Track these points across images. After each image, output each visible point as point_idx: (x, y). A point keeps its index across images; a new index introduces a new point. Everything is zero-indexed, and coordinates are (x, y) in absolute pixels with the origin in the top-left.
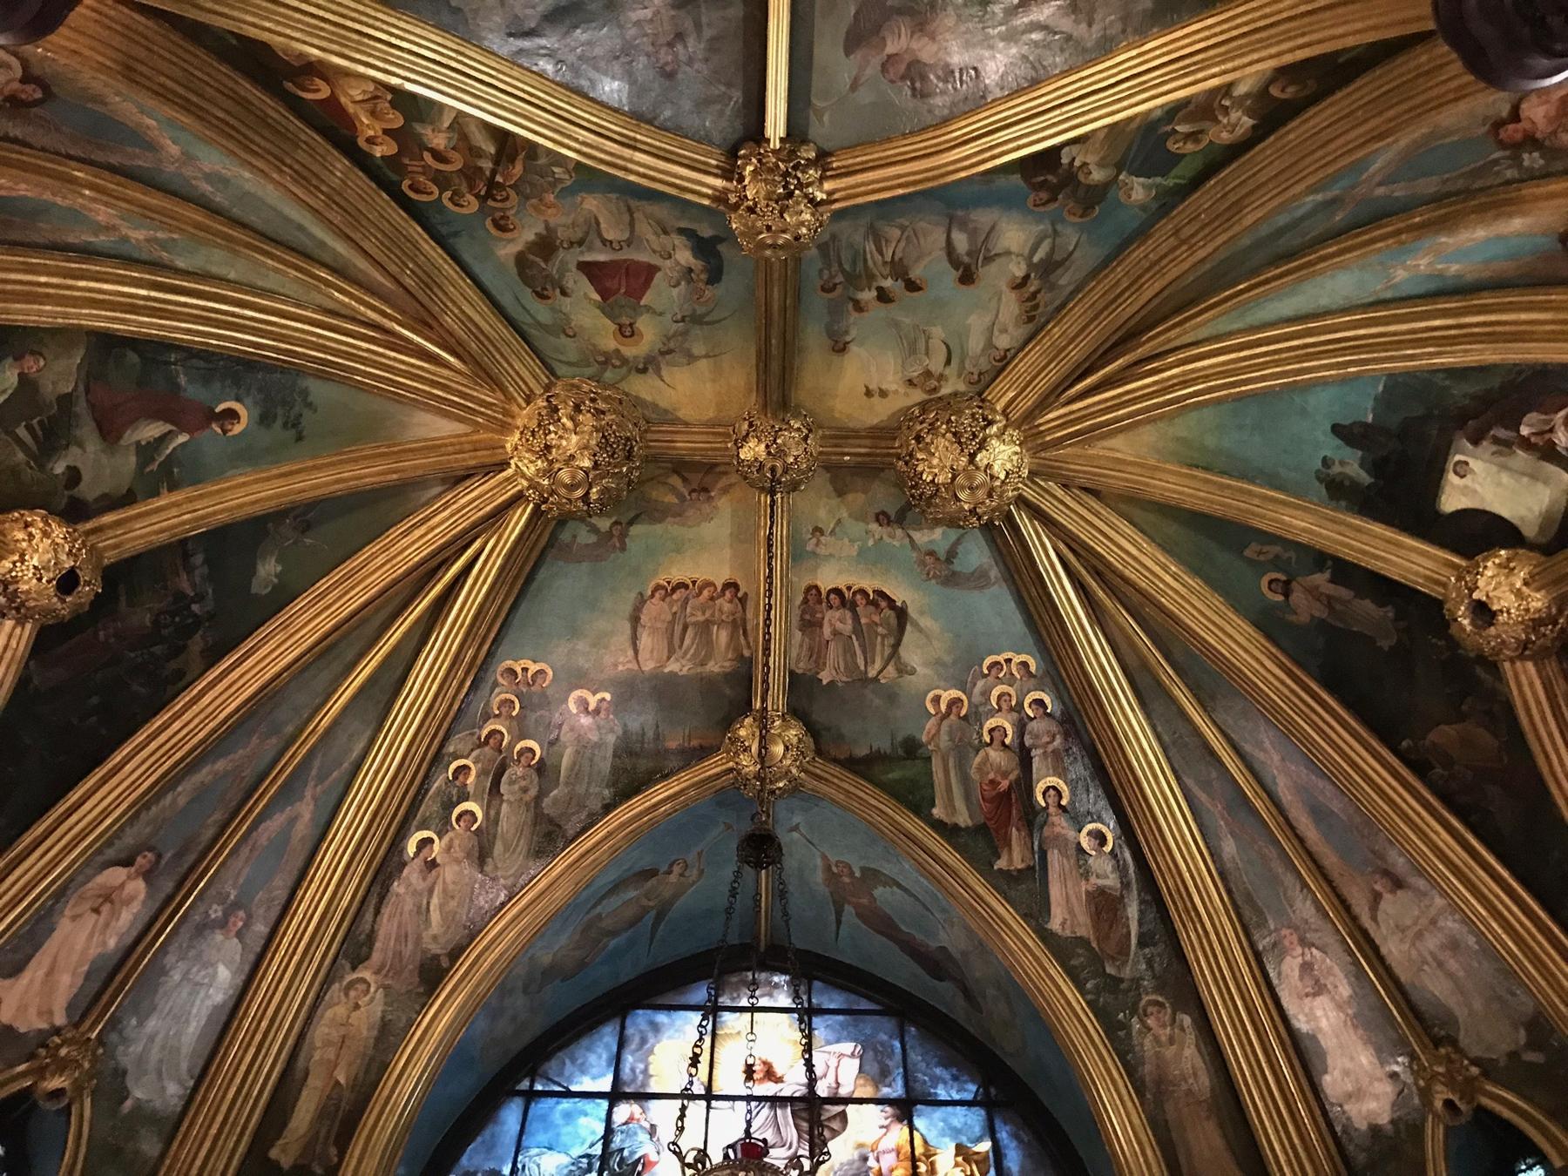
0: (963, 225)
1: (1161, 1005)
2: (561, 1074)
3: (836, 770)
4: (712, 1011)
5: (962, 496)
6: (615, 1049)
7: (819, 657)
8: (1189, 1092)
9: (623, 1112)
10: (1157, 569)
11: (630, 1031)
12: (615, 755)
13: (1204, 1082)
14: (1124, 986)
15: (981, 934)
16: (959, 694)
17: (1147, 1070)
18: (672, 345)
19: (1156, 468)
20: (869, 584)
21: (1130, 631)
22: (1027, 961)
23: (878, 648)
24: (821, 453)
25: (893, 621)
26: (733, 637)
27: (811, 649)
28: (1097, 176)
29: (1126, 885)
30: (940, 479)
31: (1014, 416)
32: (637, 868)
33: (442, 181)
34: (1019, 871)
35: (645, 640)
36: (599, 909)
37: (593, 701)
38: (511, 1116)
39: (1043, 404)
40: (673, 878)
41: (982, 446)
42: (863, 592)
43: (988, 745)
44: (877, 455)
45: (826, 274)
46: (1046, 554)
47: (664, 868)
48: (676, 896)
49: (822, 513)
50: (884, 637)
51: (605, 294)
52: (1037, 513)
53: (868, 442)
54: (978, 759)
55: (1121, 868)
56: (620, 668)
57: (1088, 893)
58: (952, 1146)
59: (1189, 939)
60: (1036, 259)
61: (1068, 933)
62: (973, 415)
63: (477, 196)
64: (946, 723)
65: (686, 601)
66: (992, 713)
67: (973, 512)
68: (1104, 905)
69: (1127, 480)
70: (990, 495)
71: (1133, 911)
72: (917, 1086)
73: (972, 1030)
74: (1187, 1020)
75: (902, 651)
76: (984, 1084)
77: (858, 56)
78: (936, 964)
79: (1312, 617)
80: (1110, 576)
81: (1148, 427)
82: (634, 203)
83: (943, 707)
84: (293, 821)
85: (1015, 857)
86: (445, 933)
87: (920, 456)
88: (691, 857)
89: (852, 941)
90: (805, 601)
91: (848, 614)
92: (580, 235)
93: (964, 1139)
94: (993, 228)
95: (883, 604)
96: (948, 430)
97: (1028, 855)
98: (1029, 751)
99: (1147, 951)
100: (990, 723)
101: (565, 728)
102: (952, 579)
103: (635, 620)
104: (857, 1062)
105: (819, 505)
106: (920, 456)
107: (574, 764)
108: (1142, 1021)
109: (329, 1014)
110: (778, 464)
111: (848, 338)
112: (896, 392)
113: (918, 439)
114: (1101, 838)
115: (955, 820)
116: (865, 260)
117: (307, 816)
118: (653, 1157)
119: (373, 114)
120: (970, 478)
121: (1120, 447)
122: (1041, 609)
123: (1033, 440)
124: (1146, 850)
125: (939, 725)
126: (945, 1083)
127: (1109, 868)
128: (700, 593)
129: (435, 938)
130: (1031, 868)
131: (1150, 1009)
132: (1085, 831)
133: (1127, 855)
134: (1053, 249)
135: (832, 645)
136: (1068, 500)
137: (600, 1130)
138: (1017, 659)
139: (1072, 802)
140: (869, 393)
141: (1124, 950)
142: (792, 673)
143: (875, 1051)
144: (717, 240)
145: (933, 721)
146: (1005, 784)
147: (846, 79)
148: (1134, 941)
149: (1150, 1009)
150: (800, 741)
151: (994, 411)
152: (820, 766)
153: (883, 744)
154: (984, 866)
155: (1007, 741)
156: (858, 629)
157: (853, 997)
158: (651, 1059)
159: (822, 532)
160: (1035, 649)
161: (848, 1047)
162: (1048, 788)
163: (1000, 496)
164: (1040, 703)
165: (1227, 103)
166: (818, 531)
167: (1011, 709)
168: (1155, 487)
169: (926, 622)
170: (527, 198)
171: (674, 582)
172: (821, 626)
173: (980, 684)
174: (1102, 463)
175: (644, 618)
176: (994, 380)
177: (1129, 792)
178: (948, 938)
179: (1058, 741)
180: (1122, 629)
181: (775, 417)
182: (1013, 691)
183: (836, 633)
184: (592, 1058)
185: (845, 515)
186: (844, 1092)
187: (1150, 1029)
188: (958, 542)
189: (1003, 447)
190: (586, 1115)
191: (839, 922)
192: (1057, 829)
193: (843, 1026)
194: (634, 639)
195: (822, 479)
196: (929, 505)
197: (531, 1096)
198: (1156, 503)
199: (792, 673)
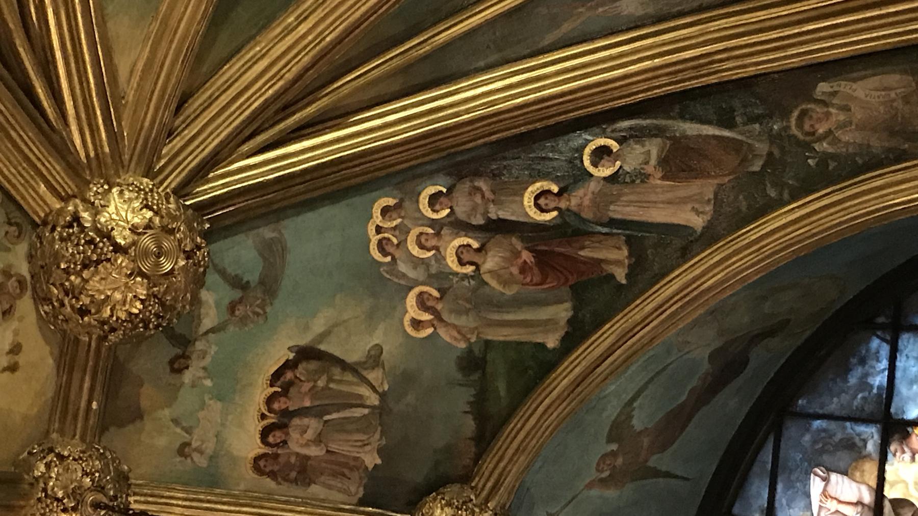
1: (804, 114)
3: (488, 464)
5: (167, 267)
7: (346, 465)
8: (906, 99)
10: (289, 40)
13: (896, 79)
14: (776, 152)
15: (701, 311)
16: (411, 300)
17: (877, 143)
19: (165, 23)
20: (261, 391)
21: (361, 81)
22: (737, 263)
23: (344, 388)
24: (83, 439)
25: (313, 365)
27: (335, 474)
29: (658, 132)
30: (142, 292)
31: (70, 186)
34: (630, 255)
39: (61, 148)
41: (107, 235)
42: (270, 400)
43: (478, 267)
44: (96, 365)
46: (253, 168)
49: (162, 441)
50: (331, 380)
52: (201, 173)
53: (77, 376)
54: (493, 283)
55: (638, 135)
57: (663, 178)
59: (730, 71)
61: (709, 208)
62: (62, 239)
64: (445, 316)
66: (440, 258)
67: (189, 255)
68: (680, 162)
69: (173, 64)
70: (172, 232)
71: (691, 129)
72: (869, 408)
73: (808, 333)
74: (823, 87)
75: (352, 357)
76: (871, 328)
78: (728, 366)
80: (289, 97)
81: (110, 25)
83: (426, 317)
85: (615, 258)
87: (107, 312)
90: (273, 475)
91: (296, 421)
95: (289, 375)
96: (79, 274)
97: (612, 241)
99: (739, 120)
100: (452, 262)
102: (269, 286)
104: (834, 477)
105: (151, 444)
106: (107, 312)
108: (820, 139)
110: (90, 498)
112: (16, 333)
114: (601, 153)
115: (563, 322)
120: (146, 253)
121: (130, 61)
122: (321, 182)
123: (105, 170)
124: (622, 102)
125: (447, 324)
130: (629, 241)
132: (591, 169)
133: (626, 124)
135: (333, 447)
136: (188, 133)
138: (377, 219)
139: (556, 180)
140: (12, 368)
141: (736, 146)
142: (362, 502)
143: (822, 451)
145: (442, 332)
146: (526, 256)
148: (726, 133)
149: (807, 127)
150: (449, 504)
151: (60, 212)
152: (483, 480)
153: (463, 397)
154: (622, 296)
155: (475, 245)
156: (318, 412)
157: (756, 469)
159: (187, 444)
160: (368, 197)
161: (816, 485)
162: (537, 205)
163: (174, 218)
164: (434, 199)
166: (183, 450)
167: (438, 234)
168: (187, 30)
169: (318, 326)
172: (308, 458)
173: (402, 267)
174: (148, 87)
176: (20, 207)
177: (553, 111)
178: (701, 351)
179: (481, 184)
180: (358, 90)
181: (26, 496)
182: (422, 235)
183: (318, 440)
185: (167, 412)
186: (868, 498)
187: (829, 132)
188: (222, 273)
189: (111, 209)
191: (667, 475)
192: (586, 202)
193: (789, 486)
195: (116, 439)
196: (173, 308)
198: (208, 28)
199: (362, 502)
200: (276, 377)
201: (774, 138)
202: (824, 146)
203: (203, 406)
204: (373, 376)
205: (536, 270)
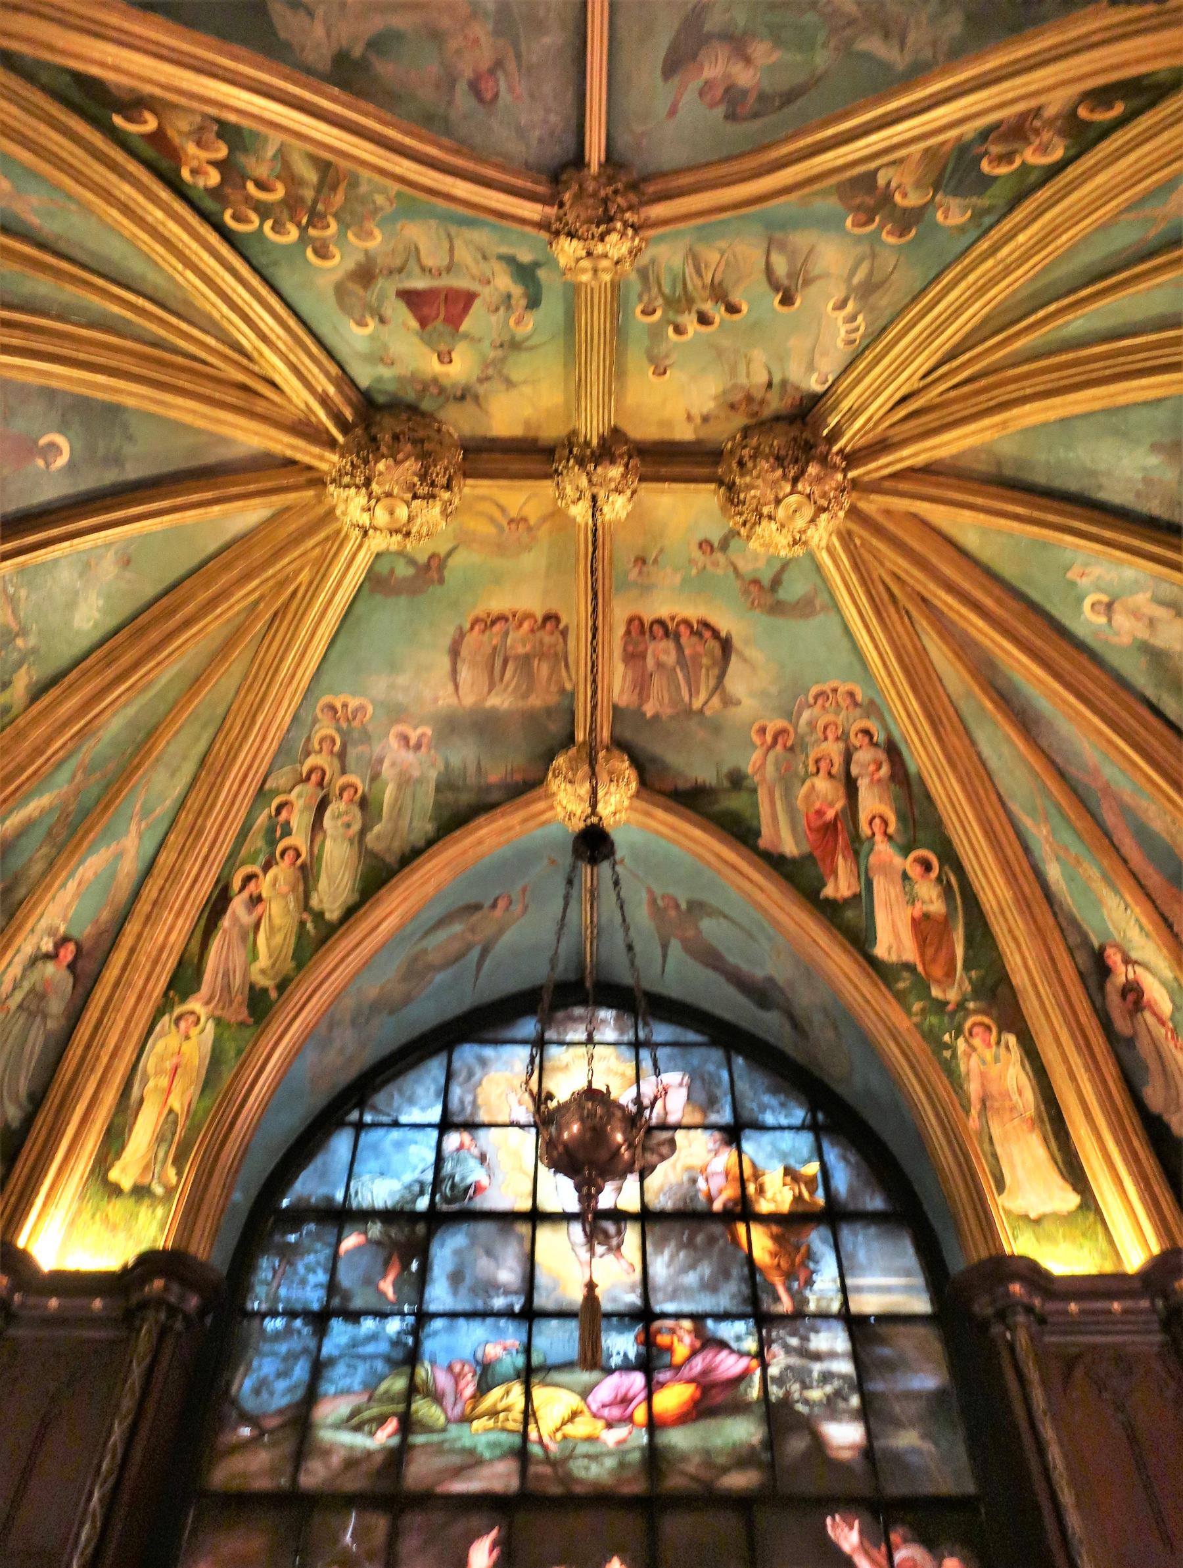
0: (782, 247)
2: (390, 1105)
4: (540, 1044)
6: (442, 1081)
9: (453, 1140)
11: (457, 1064)
12: (438, 790)
18: (490, 371)
26: (553, 671)
28: (913, 200)
32: (461, 903)
33: (264, 211)
35: (465, 674)
36: (425, 943)
37: (414, 737)
38: (341, 1143)
40: (498, 912)
42: (687, 622)
45: (645, 298)
47: (488, 903)
48: (501, 931)
51: (423, 322)
55: (947, 892)
56: (440, 703)
58: (781, 1171)
60: (856, 280)
63: (298, 225)
64: (771, 756)
65: (507, 634)
68: (927, 930)
74: (1012, 1039)
76: (812, 1109)
77: (676, 81)
78: (762, 994)
79: (1135, 639)
82: (453, 230)
83: (769, 738)
84: (119, 856)
86: (273, 965)
88: (516, 893)
89: (678, 975)
90: (628, 632)
92: (398, 262)
93: (792, 1162)
94: (811, 251)
95: (707, 634)
97: (854, 881)
98: (856, 780)
99: (973, 974)
101: (386, 764)
102: (777, 609)
103: (455, 653)
107: (396, 800)
109: (160, 1046)
111: (667, 362)
113: (741, 464)
116: (685, 284)
117: (132, 852)
118: (485, 1182)
119: (199, 144)
126: (773, 1111)
127: (934, 896)
128: (520, 625)
129: (263, 972)
130: (856, 897)
131: (975, 1030)
134: (871, 273)
135: (656, 679)
137: (431, 1157)
143: (703, 1080)
144: (536, 265)
147: (662, 109)
155: (834, 771)
158: (479, 1090)
165: (1037, 123)
167: (837, 739)
169: (752, 653)
170: (348, 227)
171: (495, 614)
175: (464, 652)
183: (660, 665)
184: (420, 1091)
186: (672, 1119)
187: (974, 1049)
190: (416, 1143)
191: (665, 956)
194: (454, 672)
197: (360, 1127)
200: (706, 625)
201: (961, 1005)
202: (961, 1044)
203: (676, 570)
204: (716, 701)
205: (820, 823)
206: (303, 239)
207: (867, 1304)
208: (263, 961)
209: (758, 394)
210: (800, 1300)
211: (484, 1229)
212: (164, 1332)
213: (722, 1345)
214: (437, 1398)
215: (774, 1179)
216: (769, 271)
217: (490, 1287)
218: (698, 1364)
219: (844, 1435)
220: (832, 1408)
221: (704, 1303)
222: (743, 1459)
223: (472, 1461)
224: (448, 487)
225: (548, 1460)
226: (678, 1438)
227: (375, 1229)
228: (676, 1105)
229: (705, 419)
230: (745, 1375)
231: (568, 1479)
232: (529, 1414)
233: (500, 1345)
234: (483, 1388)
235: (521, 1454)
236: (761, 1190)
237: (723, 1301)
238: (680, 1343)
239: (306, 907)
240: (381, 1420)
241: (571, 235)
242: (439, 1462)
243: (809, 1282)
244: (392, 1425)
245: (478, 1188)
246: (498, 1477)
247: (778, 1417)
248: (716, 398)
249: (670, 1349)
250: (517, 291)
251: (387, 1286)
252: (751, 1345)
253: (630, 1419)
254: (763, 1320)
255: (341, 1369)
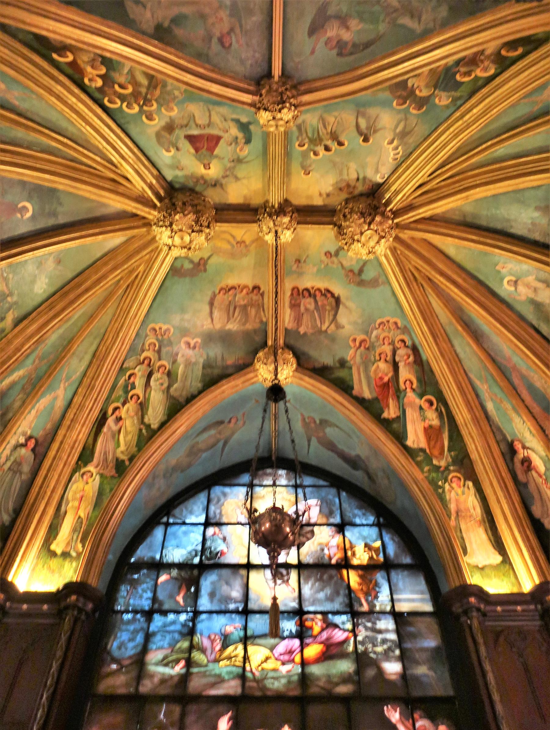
0: (364, 115)
2: (181, 514)
4: (251, 486)
6: (206, 503)
9: (211, 531)
11: (212, 496)
12: (204, 368)
18: (228, 173)
26: (257, 312)
28: (424, 93)
32: (214, 421)
33: (123, 98)
35: (216, 314)
36: (197, 439)
37: (192, 343)
38: (159, 532)
40: (232, 425)
42: (319, 290)
45: (300, 139)
47: (227, 421)
48: (233, 433)
51: (197, 150)
55: (440, 415)
56: (205, 327)
58: (363, 545)
60: (398, 130)
63: (139, 105)
64: (359, 352)
65: (236, 295)
68: (431, 433)
74: (470, 484)
76: (378, 517)
77: (314, 37)
78: (354, 463)
79: (528, 297)
82: (211, 107)
83: (357, 344)
84: (55, 398)
86: (127, 449)
88: (240, 416)
89: (315, 454)
90: (292, 294)
92: (185, 122)
93: (368, 541)
94: (377, 117)
95: (329, 295)
97: (397, 410)
98: (398, 363)
99: (453, 453)
101: (180, 356)
102: (361, 283)
103: (211, 304)
107: (184, 372)
109: (74, 487)
111: (310, 169)
113: (345, 216)
116: (318, 132)
117: (61, 396)
118: (225, 550)
119: (93, 67)
126: (360, 517)
127: (434, 417)
128: (242, 291)
129: (122, 452)
130: (398, 418)
131: (453, 480)
134: (405, 127)
135: (305, 316)
137: (200, 539)
143: (327, 503)
144: (249, 123)
147: (308, 51)
155: (388, 359)
158: (223, 507)
165: (482, 57)
167: (389, 344)
169: (350, 304)
170: (162, 105)
171: (230, 286)
175: (216, 303)
183: (307, 310)
184: (195, 508)
186: (313, 521)
187: (453, 488)
190: (193, 532)
191: (309, 445)
194: (211, 313)
197: (167, 525)
200: (328, 291)
201: (447, 468)
202: (447, 486)
203: (314, 265)
204: (333, 326)
205: (381, 383)
206: (141, 111)
207: (403, 607)
208: (122, 447)
209: (352, 184)
210: (372, 605)
211: (225, 572)
212: (76, 620)
213: (336, 626)
214: (203, 651)
215: (360, 549)
216: (357, 126)
217: (228, 599)
218: (325, 635)
219: (392, 668)
220: (387, 655)
221: (328, 607)
222: (345, 679)
223: (219, 680)
224: (208, 227)
225: (255, 680)
226: (315, 670)
227: (174, 572)
228: (314, 515)
229: (328, 195)
230: (346, 640)
231: (264, 688)
232: (246, 658)
233: (232, 626)
234: (225, 646)
235: (242, 677)
236: (354, 554)
237: (336, 606)
238: (316, 625)
239: (142, 422)
240: (177, 661)
241: (266, 109)
242: (204, 681)
243: (376, 597)
244: (182, 663)
245: (222, 553)
246: (232, 688)
247: (362, 660)
248: (333, 185)
249: (311, 628)
250: (240, 135)
251: (180, 599)
252: (349, 626)
253: (293, 661)
254: (355, 614)
255: (158, 637)
